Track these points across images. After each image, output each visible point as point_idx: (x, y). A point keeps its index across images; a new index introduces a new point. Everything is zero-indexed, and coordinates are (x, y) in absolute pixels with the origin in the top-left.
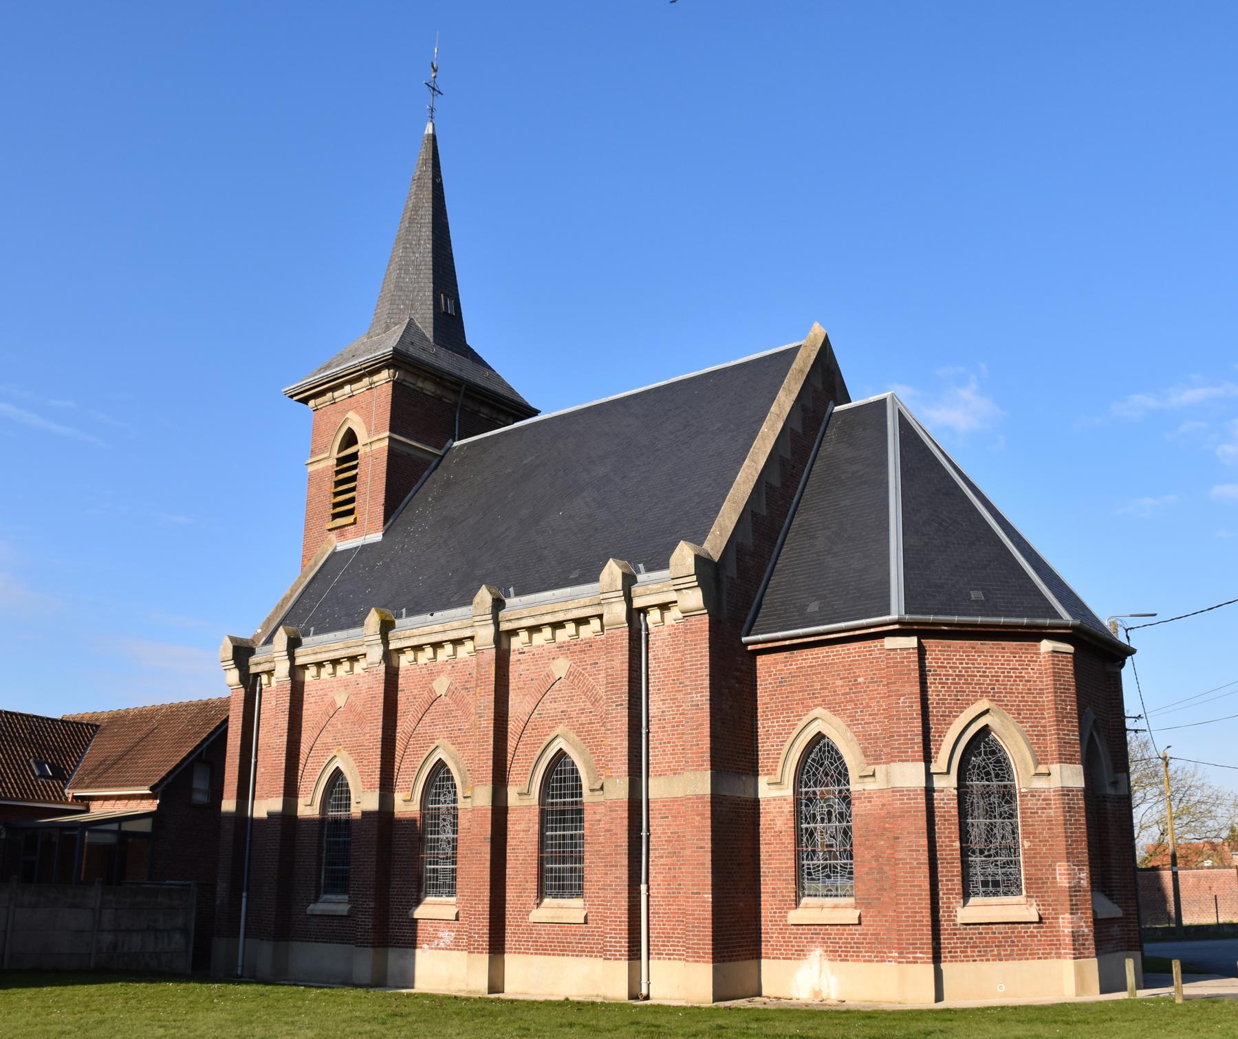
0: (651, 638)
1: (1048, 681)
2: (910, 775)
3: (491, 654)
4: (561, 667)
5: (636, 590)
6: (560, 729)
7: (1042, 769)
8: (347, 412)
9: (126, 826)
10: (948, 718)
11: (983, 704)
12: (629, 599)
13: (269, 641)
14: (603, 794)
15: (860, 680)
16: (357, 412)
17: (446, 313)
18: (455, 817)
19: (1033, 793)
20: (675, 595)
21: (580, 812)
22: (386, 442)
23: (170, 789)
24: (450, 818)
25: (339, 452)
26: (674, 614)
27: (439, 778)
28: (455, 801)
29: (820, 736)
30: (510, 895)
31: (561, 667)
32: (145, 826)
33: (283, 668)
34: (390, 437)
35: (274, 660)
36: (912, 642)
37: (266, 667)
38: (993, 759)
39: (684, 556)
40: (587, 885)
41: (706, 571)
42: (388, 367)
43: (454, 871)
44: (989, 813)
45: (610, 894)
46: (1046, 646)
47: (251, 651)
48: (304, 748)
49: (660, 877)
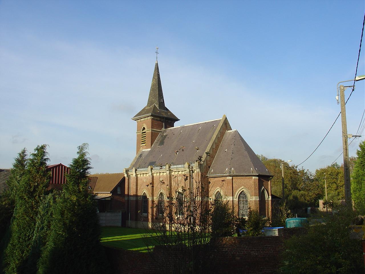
1: (253, 184)
2: (230, 198)
3: (169, 175)
7: (252, 197)
9: (106, 199)
10: (237, 190)
11: (243, 187)
13: (132, 169)
19: (250, 201)
22: (151, 131)
23: (114, 192)
25: (142, 131)
32: (109, 199)
33: (134, 174)
34: (152, 130)
35: (133, 174)
36: (231, 178)
37: (132, 174)
38: (244, 195)
42: (150, 116)
44: (243, 204)
46: (253, 178)
47: (128, 171)
48: (138, 188)
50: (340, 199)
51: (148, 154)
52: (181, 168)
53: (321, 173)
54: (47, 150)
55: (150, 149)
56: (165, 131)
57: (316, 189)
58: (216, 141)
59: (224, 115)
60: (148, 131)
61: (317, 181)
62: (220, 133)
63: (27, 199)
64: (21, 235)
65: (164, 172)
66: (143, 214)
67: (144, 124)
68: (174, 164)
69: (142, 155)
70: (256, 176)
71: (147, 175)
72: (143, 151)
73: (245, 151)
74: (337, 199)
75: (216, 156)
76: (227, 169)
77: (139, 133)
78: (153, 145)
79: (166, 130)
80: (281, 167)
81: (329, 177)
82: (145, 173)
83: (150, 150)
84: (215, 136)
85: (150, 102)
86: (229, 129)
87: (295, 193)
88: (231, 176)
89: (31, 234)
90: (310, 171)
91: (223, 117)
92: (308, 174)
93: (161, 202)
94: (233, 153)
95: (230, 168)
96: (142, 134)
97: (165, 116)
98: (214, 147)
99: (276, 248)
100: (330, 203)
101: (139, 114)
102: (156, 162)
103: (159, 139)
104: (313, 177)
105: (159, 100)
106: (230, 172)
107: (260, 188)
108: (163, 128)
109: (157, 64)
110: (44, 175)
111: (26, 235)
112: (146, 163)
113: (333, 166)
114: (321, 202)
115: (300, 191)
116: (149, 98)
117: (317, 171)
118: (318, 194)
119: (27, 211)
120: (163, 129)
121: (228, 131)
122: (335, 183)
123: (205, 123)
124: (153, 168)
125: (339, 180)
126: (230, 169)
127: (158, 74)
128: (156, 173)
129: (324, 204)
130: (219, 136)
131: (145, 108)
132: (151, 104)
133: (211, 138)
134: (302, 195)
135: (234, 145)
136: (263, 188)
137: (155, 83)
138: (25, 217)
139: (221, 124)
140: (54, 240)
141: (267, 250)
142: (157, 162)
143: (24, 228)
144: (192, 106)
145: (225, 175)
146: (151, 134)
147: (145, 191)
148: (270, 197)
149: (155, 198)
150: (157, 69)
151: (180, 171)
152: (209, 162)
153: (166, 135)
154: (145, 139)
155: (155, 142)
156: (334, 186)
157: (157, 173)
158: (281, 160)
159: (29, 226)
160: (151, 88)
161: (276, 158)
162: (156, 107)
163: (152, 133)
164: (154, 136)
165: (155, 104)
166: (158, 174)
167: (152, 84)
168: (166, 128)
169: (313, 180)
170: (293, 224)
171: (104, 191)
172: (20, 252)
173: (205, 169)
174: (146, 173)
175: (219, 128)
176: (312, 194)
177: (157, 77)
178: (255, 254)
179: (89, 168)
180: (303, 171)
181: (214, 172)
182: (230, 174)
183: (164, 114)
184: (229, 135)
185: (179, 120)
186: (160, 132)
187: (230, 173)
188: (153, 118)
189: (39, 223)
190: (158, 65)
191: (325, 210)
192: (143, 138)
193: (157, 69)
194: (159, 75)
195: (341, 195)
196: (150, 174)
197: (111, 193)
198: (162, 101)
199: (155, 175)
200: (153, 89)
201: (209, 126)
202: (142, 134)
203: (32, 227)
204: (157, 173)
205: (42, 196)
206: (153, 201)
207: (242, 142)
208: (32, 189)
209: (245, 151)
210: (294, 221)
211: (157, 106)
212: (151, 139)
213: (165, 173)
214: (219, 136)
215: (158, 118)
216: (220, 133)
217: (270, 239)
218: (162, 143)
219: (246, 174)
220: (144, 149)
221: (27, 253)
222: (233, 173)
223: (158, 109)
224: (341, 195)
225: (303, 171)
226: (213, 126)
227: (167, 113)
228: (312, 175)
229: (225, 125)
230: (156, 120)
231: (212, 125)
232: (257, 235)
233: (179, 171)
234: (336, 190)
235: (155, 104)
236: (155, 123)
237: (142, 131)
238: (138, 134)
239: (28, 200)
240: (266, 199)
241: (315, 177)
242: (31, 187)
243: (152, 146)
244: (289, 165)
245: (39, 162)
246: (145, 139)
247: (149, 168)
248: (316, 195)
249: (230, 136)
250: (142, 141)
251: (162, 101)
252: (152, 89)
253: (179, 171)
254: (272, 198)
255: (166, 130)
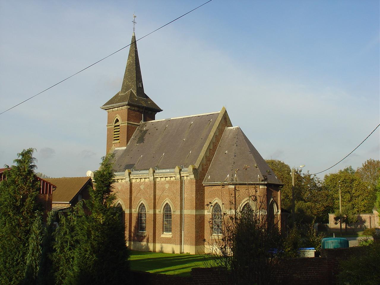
0: (185, 182)
4: (167, 186)
5: (181, 173)
6: (167, 198)
8: (116, 114)
12: (180, 174)
14: (176, 212)
15: (224, 193)
16: (119, 115)
17: (139, 87)
18: (146, 215)
20: (189, 176)
21: (171, 215)
24: (144, 215)
25: (115, 124)
26: (188, 178)
27: (142, 206)
28: (145, 211)
29: (217, 203)
30: (157, 231)
31: (167, 186)
34: (128, 123)
36: (233, 187)
39: (191, 168)
40: (172, 230)
41: (195, 171)
42: (126, 105)
43: (145, 226)
45: (176, 232)
46: (261, 187)
49: (186, 229)
50: (355, 213)
51: (123, 154)
52: (169, 174)
53: (333, 179)
54: (34, 155)
55: (126, 148)
56: (144, 125)
57: (325, 200)
58: (214, 141)
59: (224, 108)
60: (123, 124)
61: (326, 189)
62: (218, 131)
63: (12, 215)
64: (7, 260)
65: (146, 178)
66: (139, 231)
67: (117, 115)
68: (159, 168)
69: (116, 155)
70: (263, 185)
71: (123, 181)
72: (116, 149)
73: (250, 153)
74: (352, 213)
75: (213, 158)
76: (228, 176)
77: (110, 127)
78: (129, 143)
79: (146, 123)
80: (291, 173)
81: (342, 185)
82: (120, 178)
83: (126, 149)
84: (212, 134)
85: (125, 87)
86: (229, 126)
87: (299, 204)
88: (233, 185)
89: (20, 258)
90: (318, 176)
91: (222, 110)
92: (316, 180)
93: (140, 217)
94: (235, 156)
95: (232, 175)
96: (114, 127)
97: (145, 105)
98: (211, 148)
99: (319, 270)
100: (344, 218)
101: (111, 102)
102: (134, 164)
103: (136, 134)
104: (321, 185)
105: (137, 84)
106: (232, 179)
107: (268, 200)
108: (141, 121)
109: (135, 37)
110: (33, 186)
111: (13, 259)
112: (121, 165)
113: (346, 170)
114: (332, 217)
115: (305, 202)
116: (124, 81)
117: (326, 177)
118: (327, 206)
119: (13, 230)
120: (142, 122)
121: (228, 128)
122: (349, 192)
123: (199, 116)
124: (131, 173)
125: (354, 189)
126: (233, 176)
127: (135, 50)
128: (136, 179)
129: (336, 219)
130: (217, 134)
131: (118, 94)
132: (127, 90)
133: (207, 136)
134: (308, 207)
135: (237, 145)
136: (272, 199)
137: (132, 62)
138: (12, 237)
139: (220, 118)
140: (80, 264)
141: (310, 273)
142: (136, 164)
143: (11, 251)
144: (181, 95)
145: (226, 183)
146: (127, 128)
147: (119, 202)
148: (280, 211)
149: (133, 210)
150: (134, 43)
151: (167, 177)
152: (205, 167)
153: (147, 130)
154: (119, 134)
155: (131, 138)
156: (348, 196)
157: (137, 179)
158: (280, 162)
159: (17, 249)
160: (126, 68)
161: (273, 159)
162: (133, 93)
163: (128, 127)
164: (130, 130)
165: (131, 89)
166: (138, 180)
167: (127, 63)
168: (145, 120)
169: (320, 189)
170: (331, 245)
171: (57, 201)
172: (7, 279)
173: (200, 175)
174: (122, 178)
175: (217, 124)
176: (320, 207)
177: (134, 55)
178: (297, 277)
179: (114, 181)
180: (309, 176)
181: (212, 179)
182: (232, 182)
183: (143, 103)
184: (230, 133)
185: (162, 110)
186: (138, 125)
187: (232, 180)
188: (130, 107)
189: (34, 244)
190: (135, 38)
191: (338, 226)
192: (116, 133)
193: (134, 43)
194: (136, 52)
195: (356, 208)
196: (128, 179)
197: (70, 203)
198: (141, 86)
199: (134, 181)
200: (129, 69)
201: (203, 122)
202: (115, 128)
203: (21, 249)
204: (137, 179)
205: (37, 213)
206: (131, 214)
207: (247, 142)
208: (18, 204)
209: (250, 153)
210: (333, 241)
211: (134, 92)
212: (127, 134)
213: (148, 179)
214: (217, 134)
215: (136, 108)
216: (218, 131)
217: (314, 260)
218: (141, 140)
219: (252, 183)
220: (117, 147)
221: (16, 280)
222: (236, 181)
223: (136, 96)
224: (356, 208)
225: (309, 176)
226: (209, 121)
227: (147, 102)
228: (320, 182)
229: (224, 120)
230: (134, 110)
231: (207, 120)
232: (295, 257)
233: (167, 177)
234: (349, 201)
235: (131, 89)
236: (132, 114)
237: (115, 124)
238: (109, 127)
239: (13, 216)
240: (275, 214)
241: (323, 185)
242: (17, 201)
243: (128, 144)
244: (290, 168)
245: (26, 170)
246: (119, 134)
247: (127, 172)
248: (325, 207)
249: (231, 134)
250: (114, 137)
251: (141, 86)
252: (128, 70)
253: (167, 177)
254: (282, 211)
255: (146, 123)
